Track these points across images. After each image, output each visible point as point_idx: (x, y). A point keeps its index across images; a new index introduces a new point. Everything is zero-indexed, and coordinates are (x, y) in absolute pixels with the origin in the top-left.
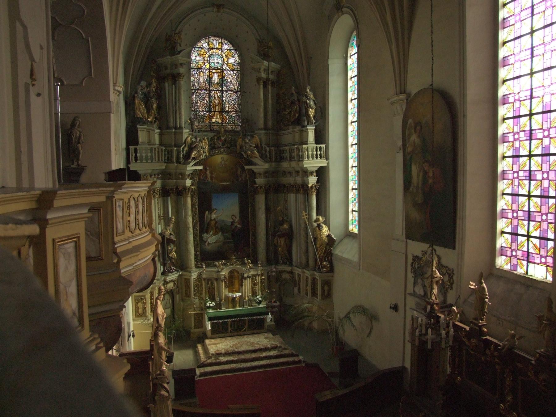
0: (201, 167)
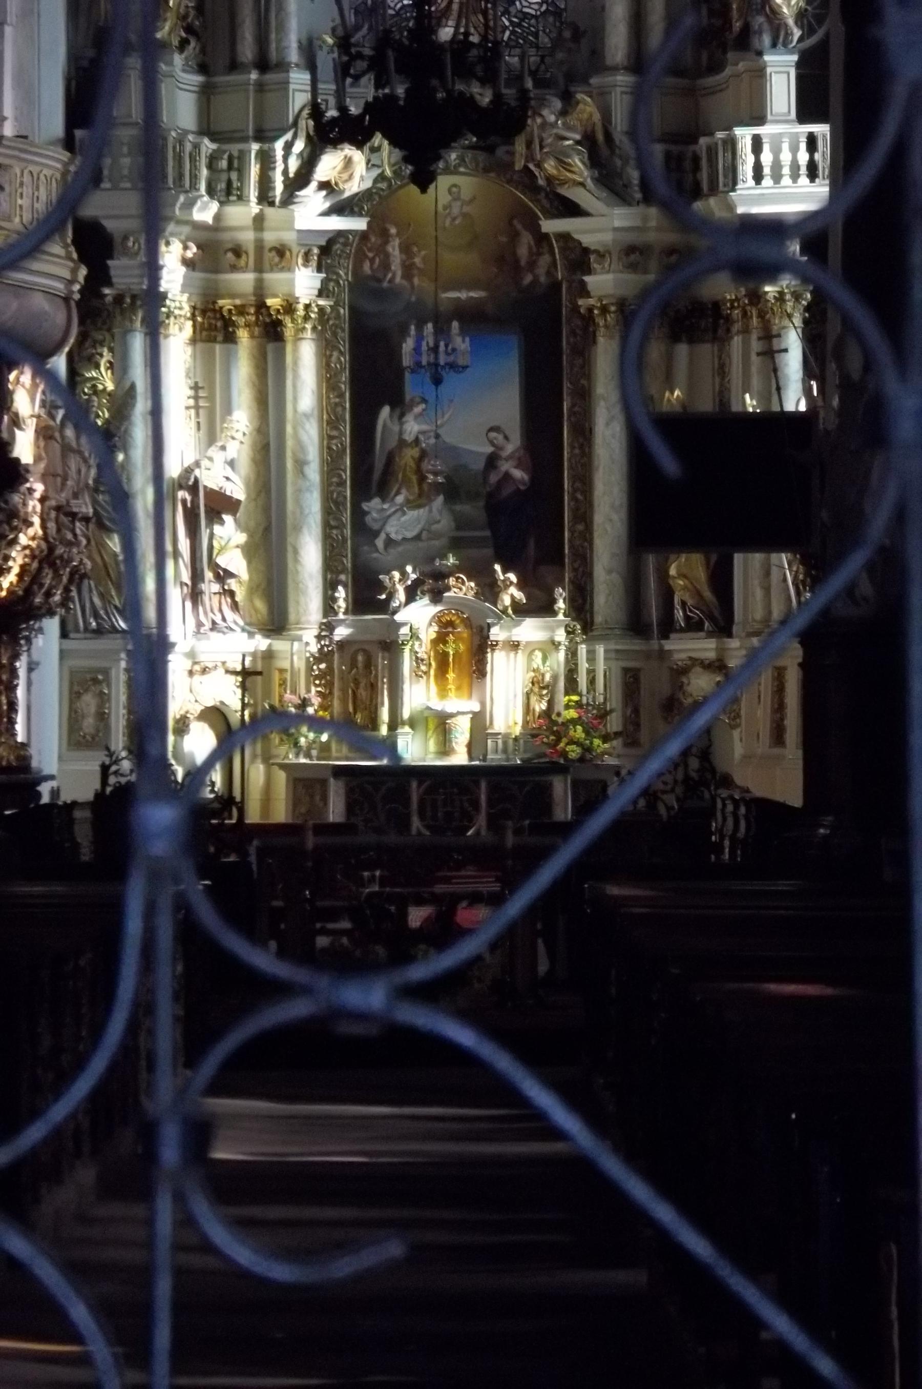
0: (359, 224)
